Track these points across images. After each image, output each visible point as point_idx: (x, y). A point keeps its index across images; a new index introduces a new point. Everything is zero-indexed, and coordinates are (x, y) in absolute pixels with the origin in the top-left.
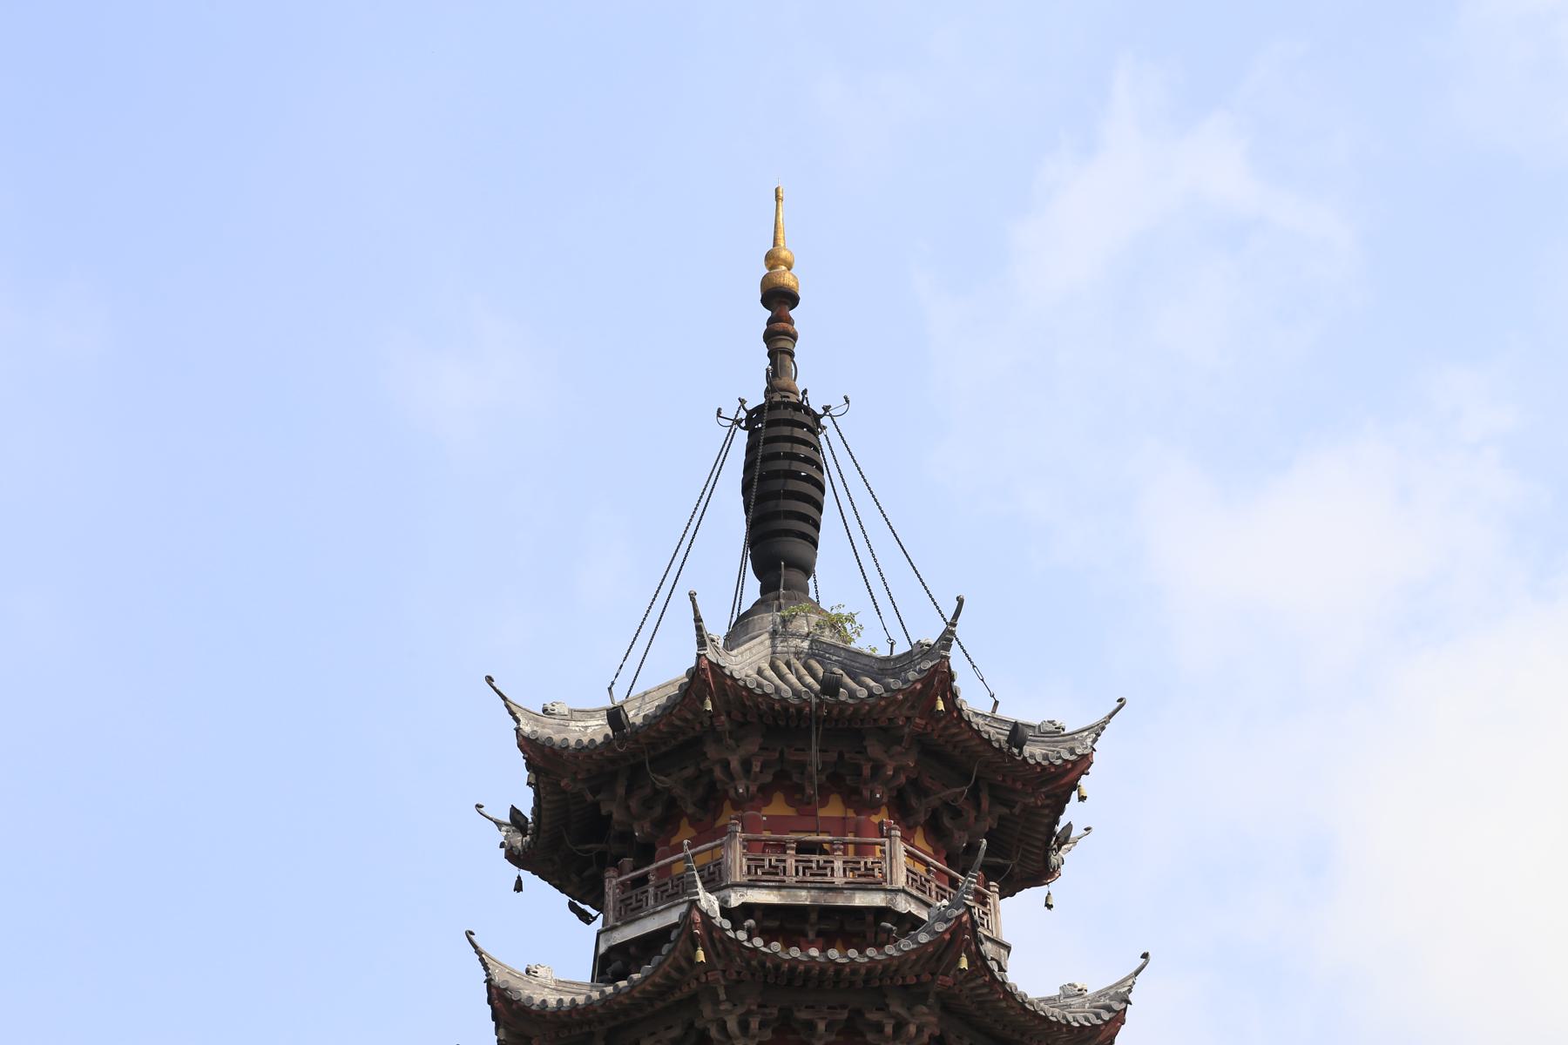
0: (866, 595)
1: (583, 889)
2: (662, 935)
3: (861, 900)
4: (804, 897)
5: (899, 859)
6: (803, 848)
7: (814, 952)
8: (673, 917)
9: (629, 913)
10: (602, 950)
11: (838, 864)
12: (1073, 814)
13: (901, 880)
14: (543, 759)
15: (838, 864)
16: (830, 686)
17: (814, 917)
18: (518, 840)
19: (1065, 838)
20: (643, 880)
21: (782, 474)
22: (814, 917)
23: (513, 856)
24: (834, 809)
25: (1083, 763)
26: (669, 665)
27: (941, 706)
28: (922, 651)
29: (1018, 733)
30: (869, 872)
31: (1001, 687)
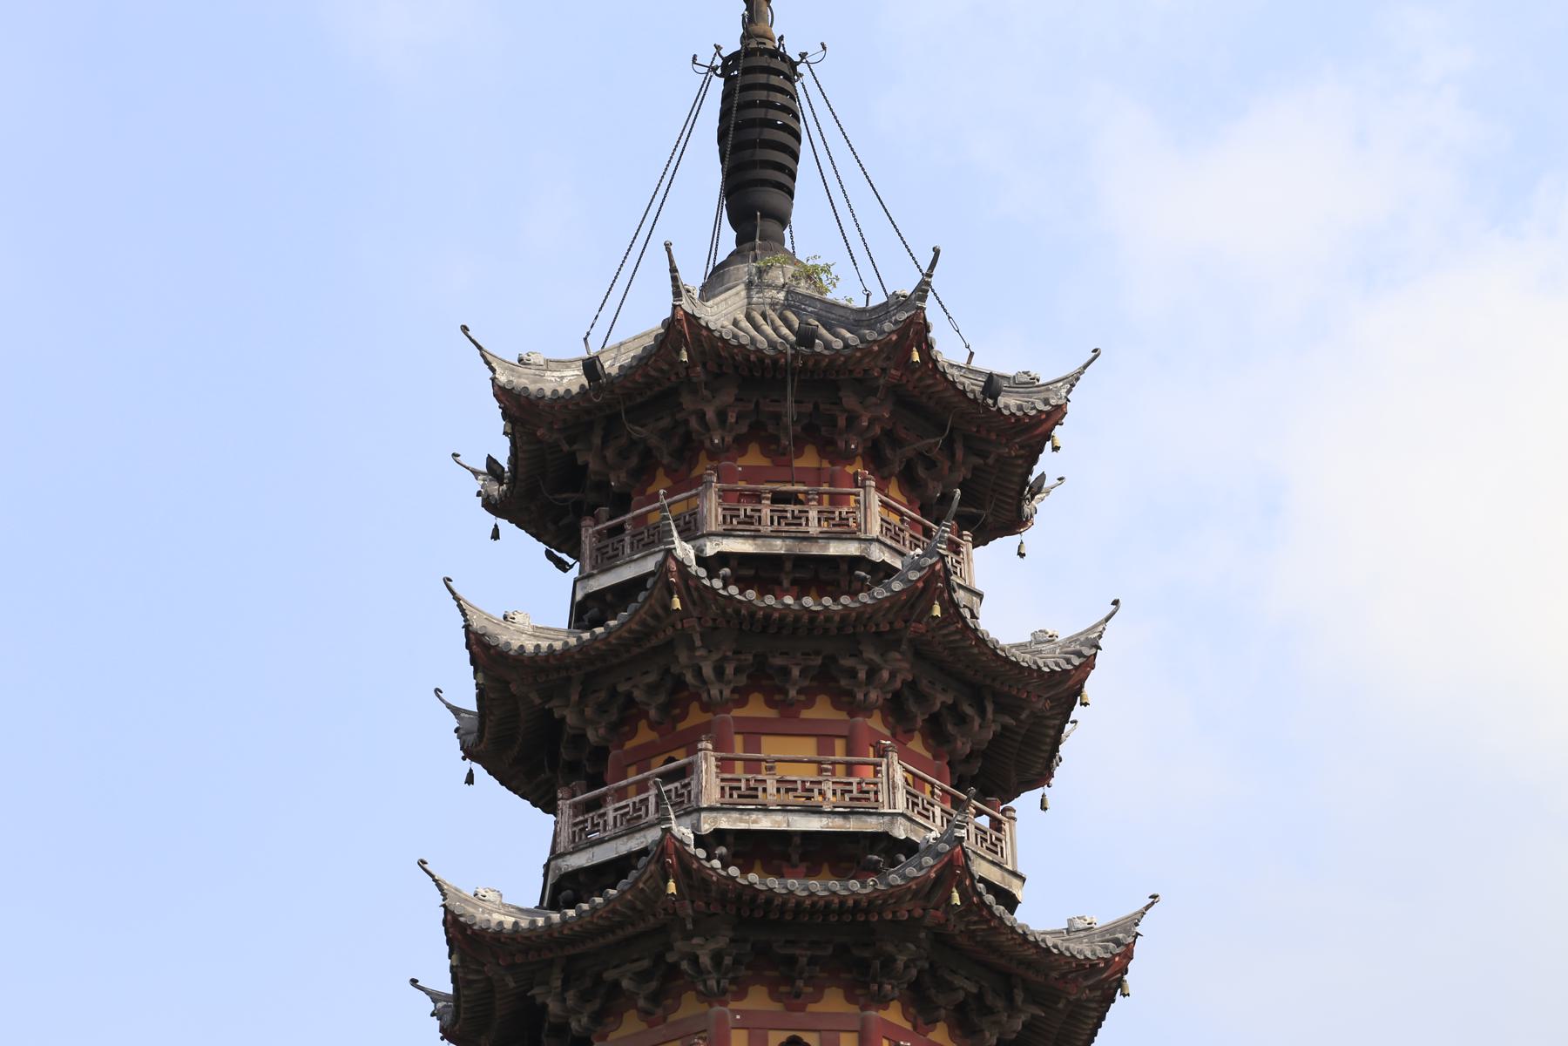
0: (842, 247)
1: (558, 536)
2: (638, 583)
3: (835, 549)
4: (779, 547)
5: (873, 509)
6: (778, 498)
7: (789, 600)
8: (649, 565)
9: (605, 561)
10: (579, 597)
11: (813, 514)
12: (1047, 463)
13: (875, 530)
14: (518, 407)
15: (813, 514)
16: (806, 337)
17: (788, 565)
18: (495, 489)
19: (1038, 488)
20: (620, 529)
21: (1100, 637)
22: (788, 565)
23: (490, 505)
24: (809, 460)
25: (1056, 414)
26: (646, 315)
27: (916, 357)
28: (898, 302)
29: (992, 384)
30: (843, 521)
31: (976, 339)
